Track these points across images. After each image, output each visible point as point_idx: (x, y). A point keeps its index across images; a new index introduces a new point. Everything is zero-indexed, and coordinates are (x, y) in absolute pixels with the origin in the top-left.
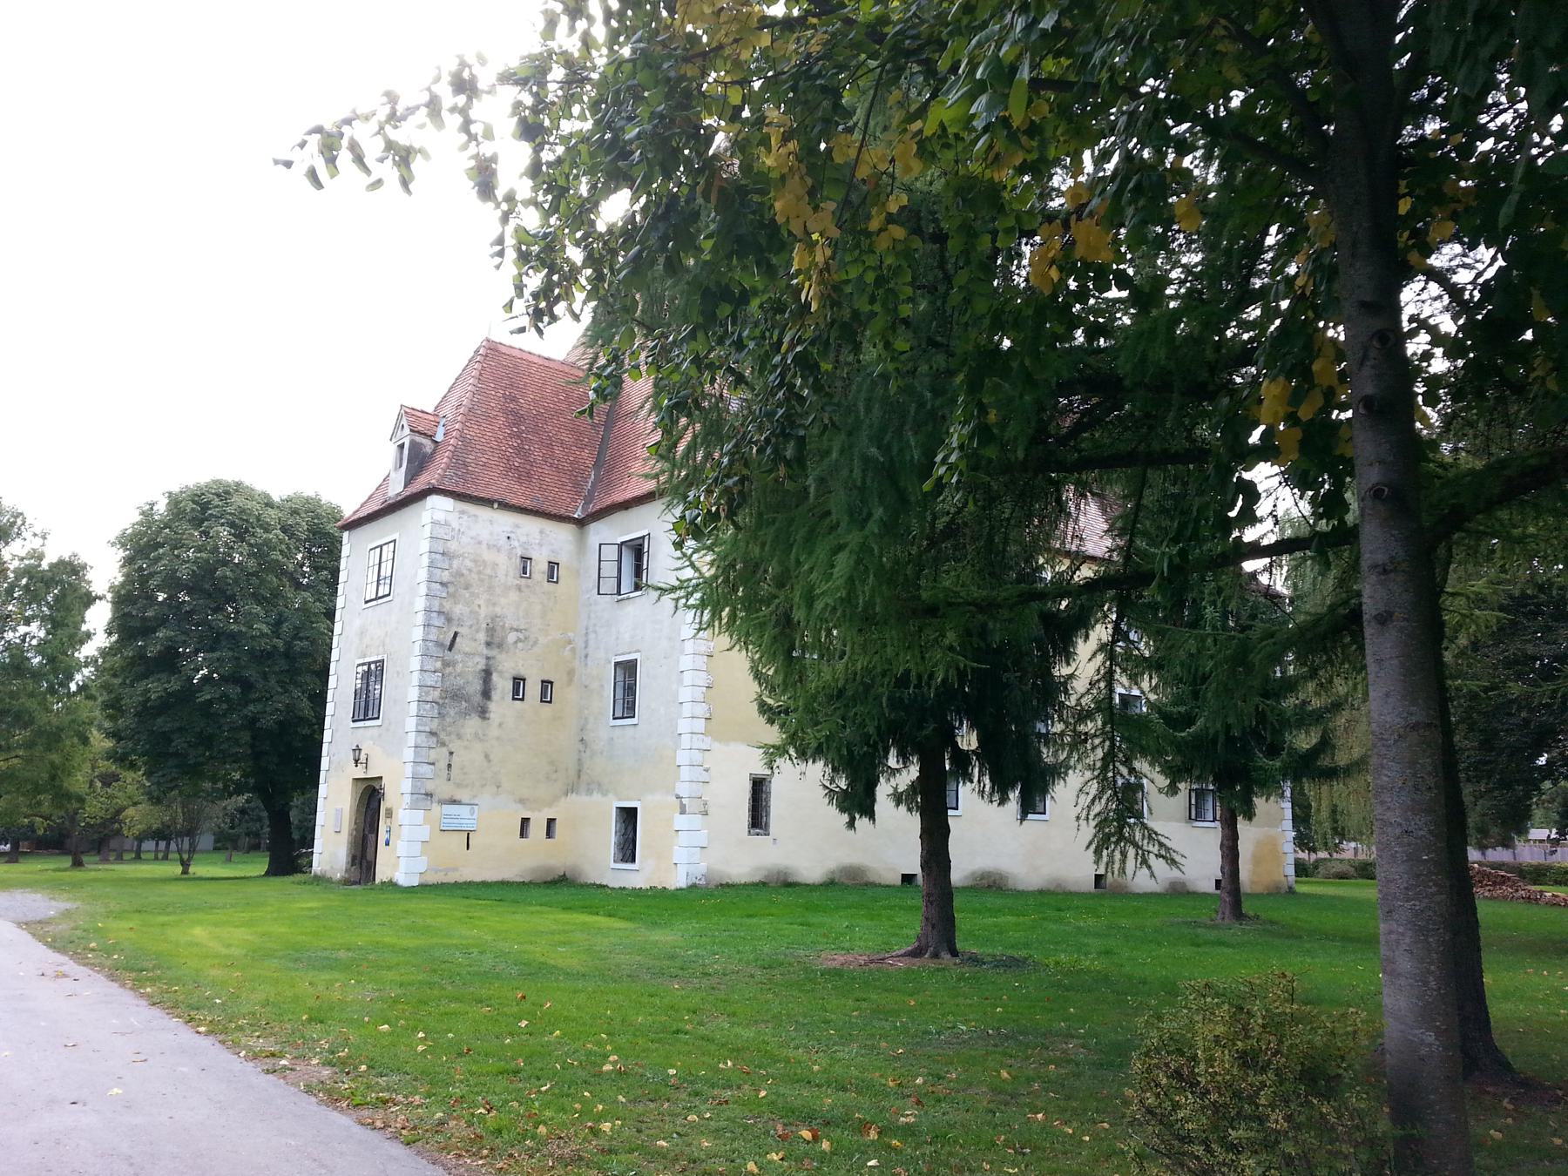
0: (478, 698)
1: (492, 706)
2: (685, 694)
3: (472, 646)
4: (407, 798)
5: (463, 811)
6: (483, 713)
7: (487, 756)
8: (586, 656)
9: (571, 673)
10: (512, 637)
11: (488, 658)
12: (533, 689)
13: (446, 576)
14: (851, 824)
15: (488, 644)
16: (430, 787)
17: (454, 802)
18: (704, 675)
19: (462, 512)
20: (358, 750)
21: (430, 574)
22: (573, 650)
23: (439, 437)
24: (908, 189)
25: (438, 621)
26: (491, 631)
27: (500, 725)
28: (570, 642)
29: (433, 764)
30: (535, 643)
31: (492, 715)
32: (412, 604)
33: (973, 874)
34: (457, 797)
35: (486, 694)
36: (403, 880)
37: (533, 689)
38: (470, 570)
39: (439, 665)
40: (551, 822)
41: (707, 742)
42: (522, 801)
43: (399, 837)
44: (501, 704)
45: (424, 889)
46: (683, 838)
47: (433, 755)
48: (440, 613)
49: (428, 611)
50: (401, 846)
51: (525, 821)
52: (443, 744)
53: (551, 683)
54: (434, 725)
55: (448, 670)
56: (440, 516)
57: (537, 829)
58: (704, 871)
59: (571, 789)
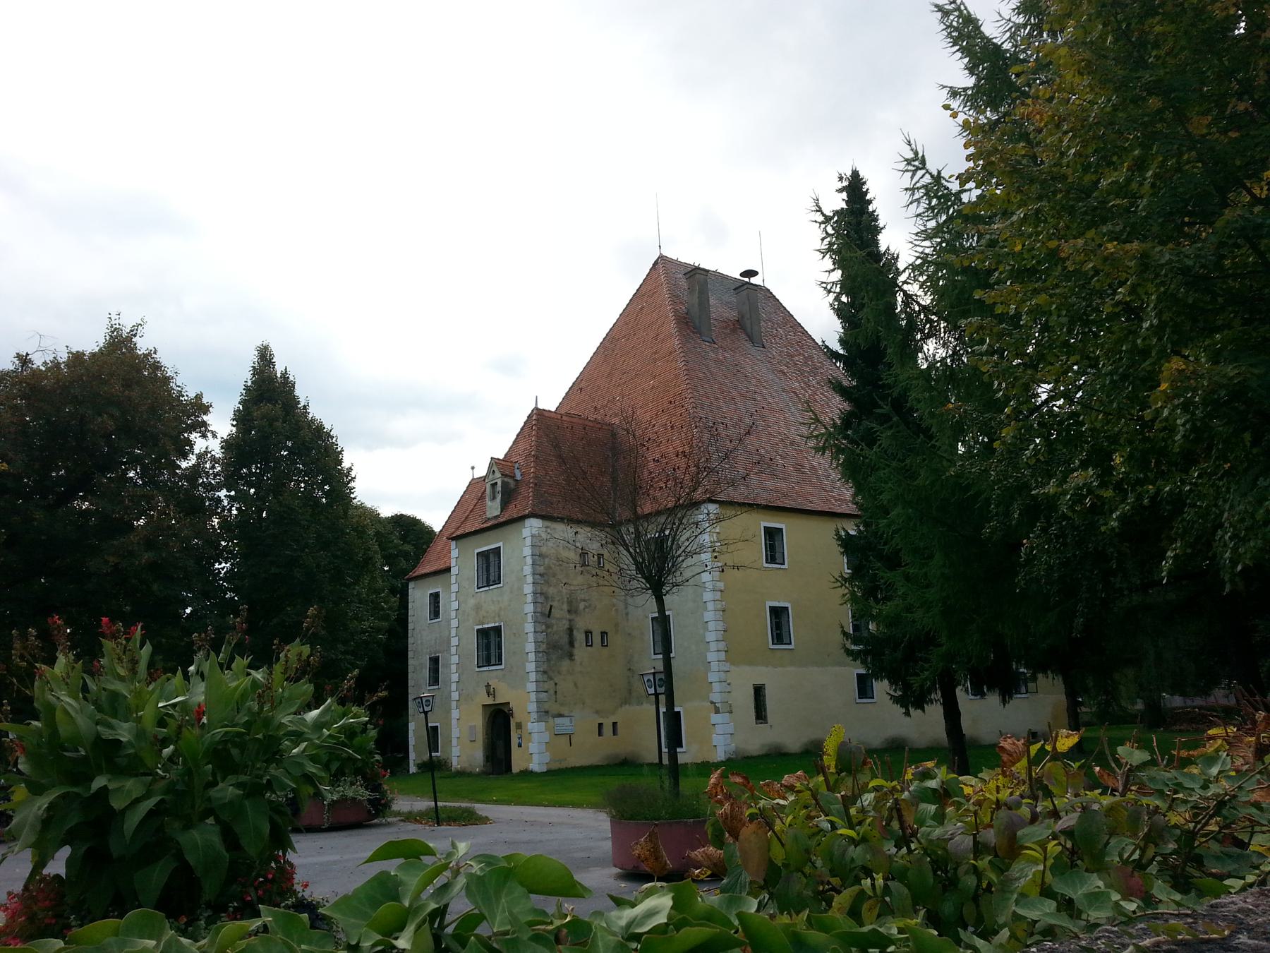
0: (567, 647)
1: (576, 652)
2: (711, 636)
3: (560, 612)
4: (535, 715)
5: (566, 721)
6: (571, 656)
7: (575, 685)
8: (627, 614)
9: (617, 625)
10: (582, 605)
11: (570, 620)
12: (597, 638)
13: (541, 570)
14: (907, 714)
15: (569, 611)
16: (546, 707)
17: (561, 715)
18: (721, 623)
19: (547, 527)
20: (488, 686)
21: (534, 569)
22: (617, 610)
23: (518, 477)
24: (64, 362)
25: (541, 600)
26: (570, 603)
27: (581, 664)
28: (614, 605)
29: (546, 692)
30: (595, 607)
31: (576, 657)
32: (521, 589)
33: (886, 740)
34: (562, 713)
35: (571, 644)
36: (536, 766)
37: (597, 638)
38: (555, 565)
39: (544, 627)
40: (615, 724)
41: (726, 667)
42: (597, 712)
43: (530, 741)
44: (580, 651)
45: (549, 773)
46: (719, 729)
47: (546, 686)
48: (541, 594)
49: (535, 593)
50: (534, 747)
51: (600, 725)
52: (551, 679)
53: (607, 633)
54: (545, 667)
55: (549, 630)
56: (535, 531)
57: (608, 730)
58: (734, 749)
59: (626, 701)
